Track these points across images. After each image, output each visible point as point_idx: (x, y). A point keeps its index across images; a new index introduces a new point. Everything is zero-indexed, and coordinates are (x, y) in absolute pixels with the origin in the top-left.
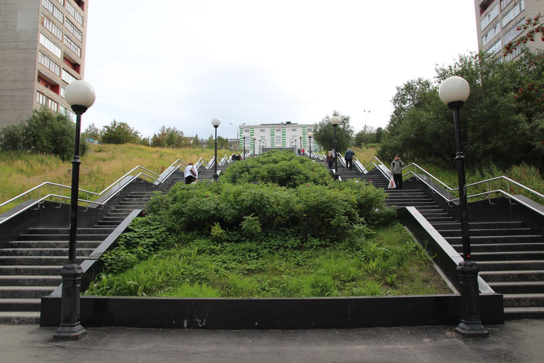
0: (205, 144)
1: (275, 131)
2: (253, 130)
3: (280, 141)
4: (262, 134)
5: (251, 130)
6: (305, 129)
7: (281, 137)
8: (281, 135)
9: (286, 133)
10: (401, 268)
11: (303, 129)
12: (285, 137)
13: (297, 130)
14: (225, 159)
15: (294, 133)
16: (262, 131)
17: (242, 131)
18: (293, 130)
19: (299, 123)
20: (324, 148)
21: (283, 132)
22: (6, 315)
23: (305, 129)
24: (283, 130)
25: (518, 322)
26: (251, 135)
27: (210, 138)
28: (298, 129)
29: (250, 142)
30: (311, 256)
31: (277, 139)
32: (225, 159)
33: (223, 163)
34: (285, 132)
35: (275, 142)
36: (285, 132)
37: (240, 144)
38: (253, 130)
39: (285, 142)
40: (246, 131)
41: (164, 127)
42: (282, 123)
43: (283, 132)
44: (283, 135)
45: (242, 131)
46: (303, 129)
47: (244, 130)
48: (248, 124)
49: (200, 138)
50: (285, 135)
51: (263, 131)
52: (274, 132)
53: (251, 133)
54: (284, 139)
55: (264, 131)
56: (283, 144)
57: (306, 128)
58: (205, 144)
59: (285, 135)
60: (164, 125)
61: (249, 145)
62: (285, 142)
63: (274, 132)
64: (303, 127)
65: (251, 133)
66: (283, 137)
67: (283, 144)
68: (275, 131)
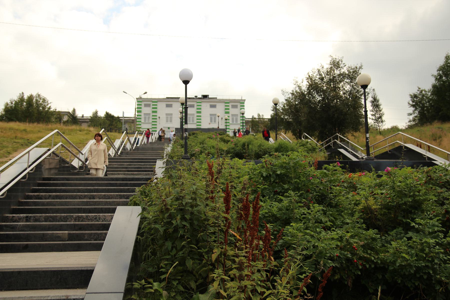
0: (87, 122)
1: (230, 107)
2: (156, 105)
3: (237, 121)
4: (169, 110)
5: (153, 105)
6: (228, 106)
7: (195, 116)
8: (150, 112)
9: (158, 110)
10: (360, 246)
11: (226, 106)
12: (200, 116)
13: (173, 106)
14: (123, 142)
15: (213, 111)
16: (168, 106)
17: (141, 105)
18: (212, 106)
19: (219, 98)
20: (340, 131)
21: (197, 109)
22: (59, 294)
23: (228, 106)
24: (198, 106)
25: (65, 296)
26: (153, 112)
27: (94, 114)
28: (218, 105)
29: (151, 122)
30: (241, 241)
31: (145, 118)
32: (123, 142)
33: (119, 149)
34: (200, 109)
35: (231, 122)
36: (200, 109)
37: (138, 123)
38: (156, 105)
39: (200, 122)
40: (146, 105)
41: (23, 93)
42: (196, 97)
43: (197, 109)
44: (198, 112)
45: (141, 105)
46: (226, 106)
47: (143, 104)
48: (152, 95)
49: (79, 114)
50: (200, 112)
51: (170, 106)
52: (228, 109)
53: (153, 108)
54: (155, 119)
55: (172, 107)
56: (153, 125)
57: (230, 105)
58: (87, 122)
59: (200, 112)
60: (23, 92)
61: (151, 125)
62: (200, 122)
63: (228, 109)
64: (226, 103)
65: (153, 108)
66: (197, 116)
67: (153, 125)
68: (230, 107)
